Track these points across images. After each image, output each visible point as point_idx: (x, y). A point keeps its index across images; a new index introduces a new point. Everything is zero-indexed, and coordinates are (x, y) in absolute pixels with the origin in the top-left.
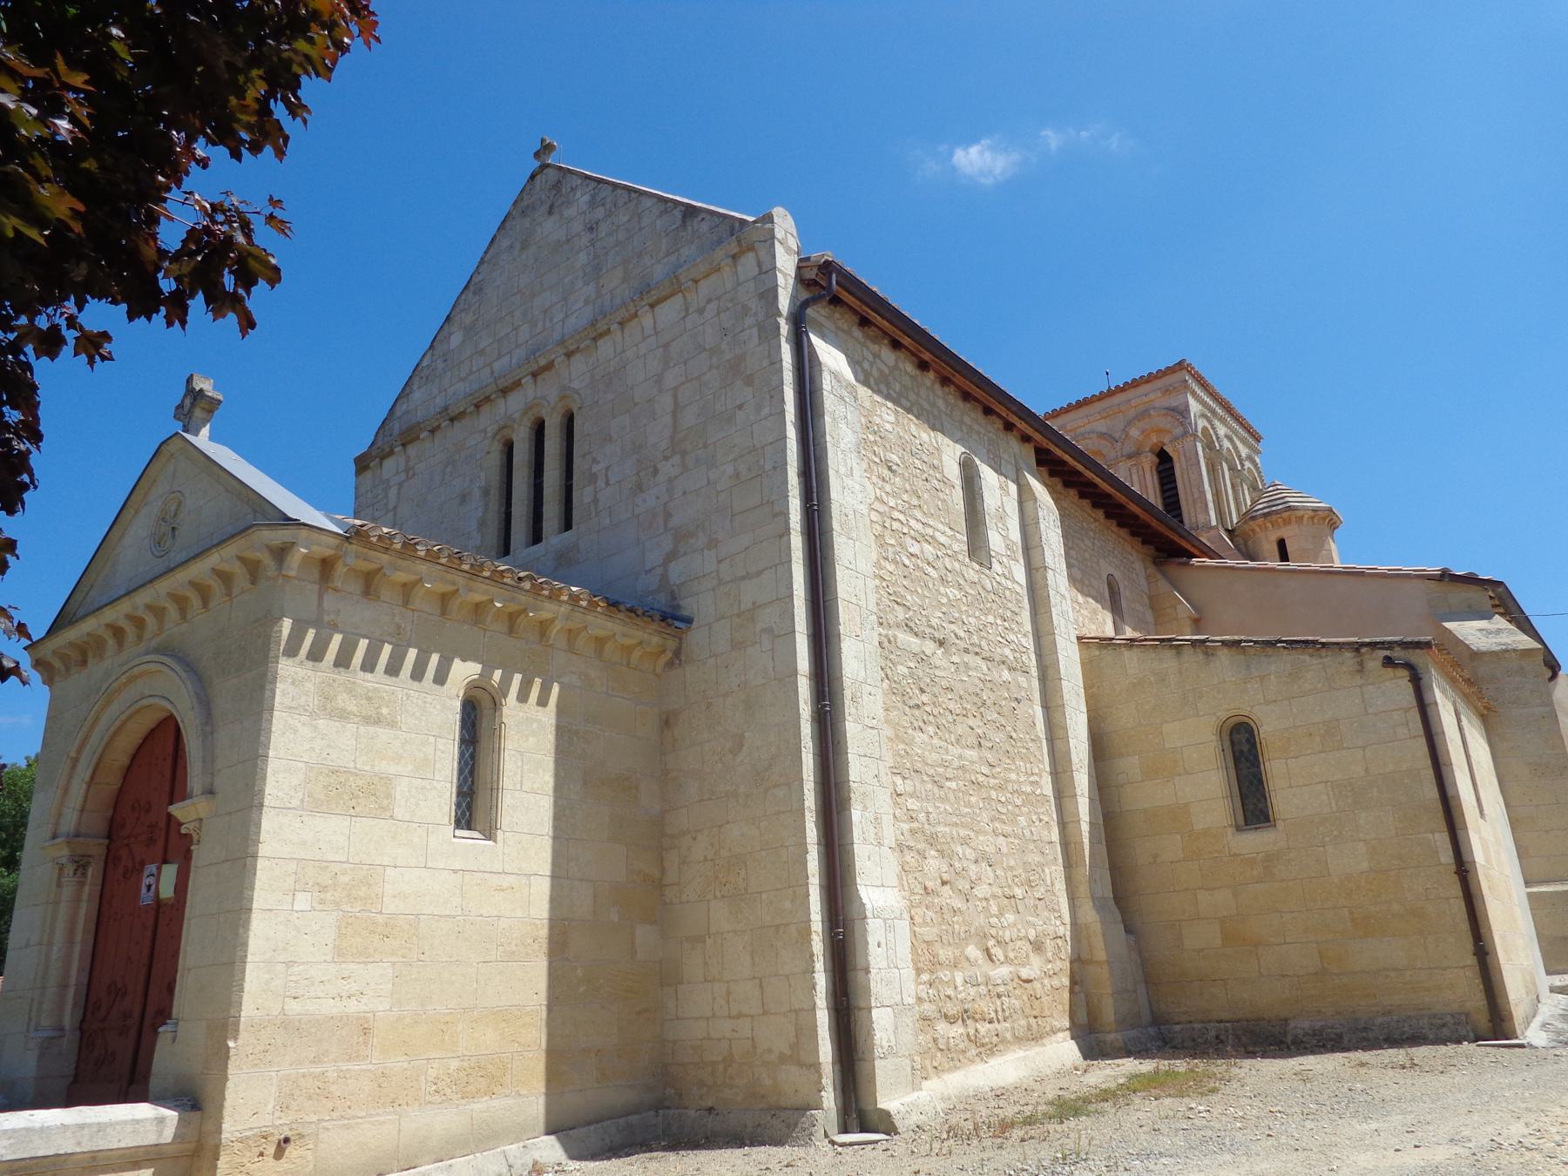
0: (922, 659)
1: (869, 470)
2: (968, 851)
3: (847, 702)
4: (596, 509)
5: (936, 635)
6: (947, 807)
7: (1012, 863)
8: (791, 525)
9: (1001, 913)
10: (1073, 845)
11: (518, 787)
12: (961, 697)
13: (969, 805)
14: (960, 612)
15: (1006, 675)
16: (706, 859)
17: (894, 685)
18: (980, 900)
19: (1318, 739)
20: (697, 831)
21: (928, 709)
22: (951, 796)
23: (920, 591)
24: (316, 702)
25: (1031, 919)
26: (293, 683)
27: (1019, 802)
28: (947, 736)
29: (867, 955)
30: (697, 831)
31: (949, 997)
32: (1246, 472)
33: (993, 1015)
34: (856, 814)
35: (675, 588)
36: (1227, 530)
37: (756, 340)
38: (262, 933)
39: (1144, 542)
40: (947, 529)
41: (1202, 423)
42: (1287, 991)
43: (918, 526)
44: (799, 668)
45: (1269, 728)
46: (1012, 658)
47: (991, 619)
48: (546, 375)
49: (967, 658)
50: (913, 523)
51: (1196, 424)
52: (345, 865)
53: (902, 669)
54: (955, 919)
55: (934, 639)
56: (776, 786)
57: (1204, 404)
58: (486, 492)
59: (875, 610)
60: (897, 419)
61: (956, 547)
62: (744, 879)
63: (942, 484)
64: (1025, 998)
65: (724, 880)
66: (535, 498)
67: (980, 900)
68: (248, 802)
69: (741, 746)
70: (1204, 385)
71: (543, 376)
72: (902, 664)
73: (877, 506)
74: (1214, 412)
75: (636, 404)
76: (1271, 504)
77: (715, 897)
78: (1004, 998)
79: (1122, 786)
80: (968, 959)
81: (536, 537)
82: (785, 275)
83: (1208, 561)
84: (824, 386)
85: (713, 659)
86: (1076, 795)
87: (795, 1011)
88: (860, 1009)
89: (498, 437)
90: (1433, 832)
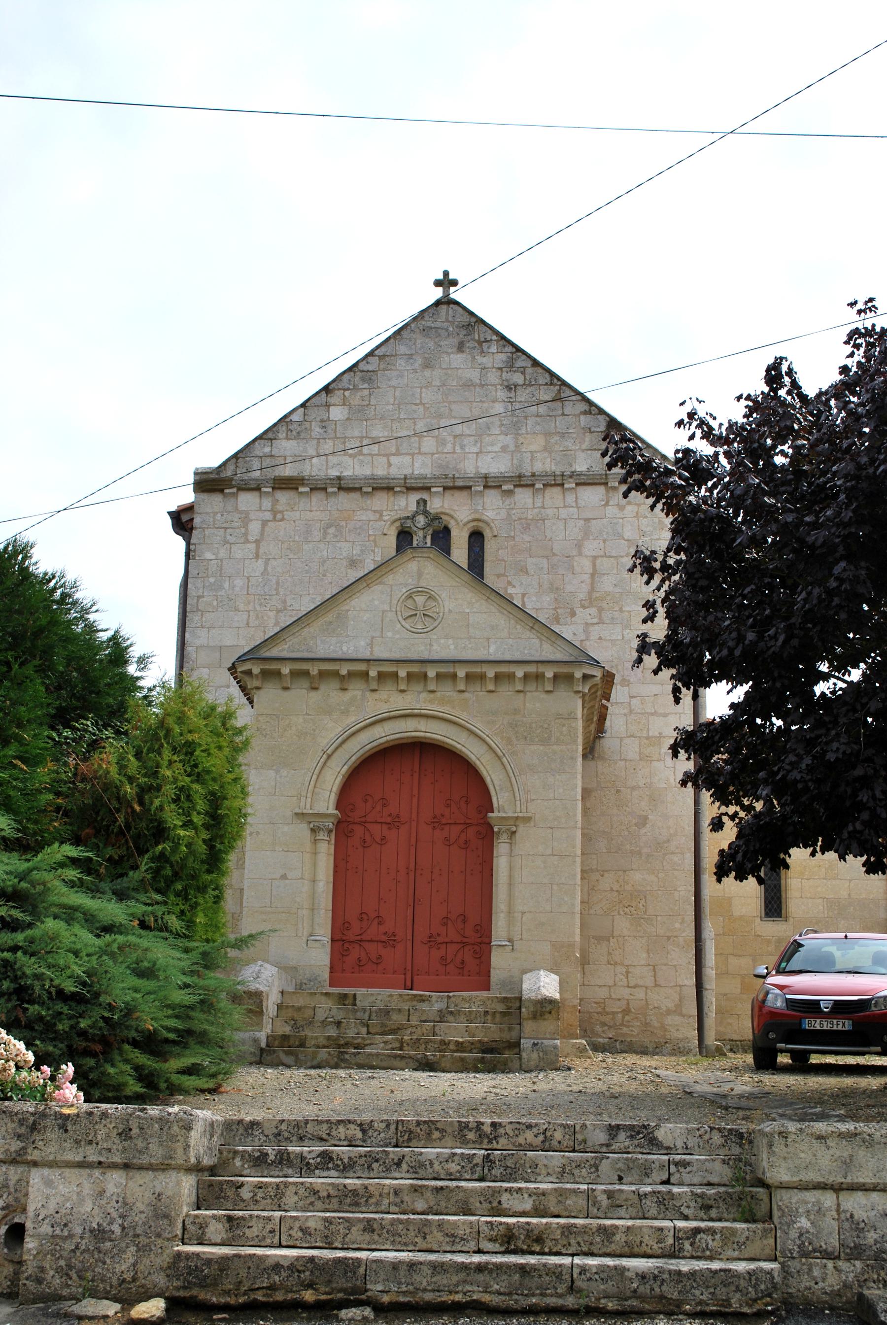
16: (612, 890)
30: (603, 871)
56: (672, 853)
69: (644, 825)
75: (554, 555)
77: (619, 914)
85: (623, 762)
87: (680, 986)
88: (706, 989)
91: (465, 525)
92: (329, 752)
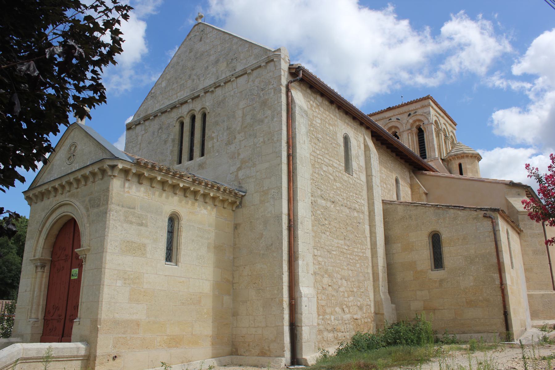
0: (326, 208)
1: (311, 141)
2: (338, 275)
3: (299, 224)
4: (213, 149)
5: (332, 200)
6: (332, 260)
7: (353, 280)
8: (283, 161)
9: (348, 297)
10: (375, 274)
11: (186, 248)
12: (339, 222)
13: (339, 260)
14: (341, 191)
15: (356, 214)
16: (248, 275)
17: (316, 218)
18: (342, 292)
19: (460, 240)
20: (245, 265)
21: (327, 226)
22: (334, 256)
23: (326, 184)
24: (123, 218)
25: (359, 299)
26: (116, 212)
27: (357, 259)
28: (333, 236)
29: (301, 309)
30: (245, 265)
31: (329, 323)
32: (450, 137)
33: (343, 330)
34: (300, 262)
35: (240, 180)
36: (441, 159)
37: (273, 93)
38: (107, 292)
39: (410, 165)
40: (338, 162)
41: (435, 118)
42: (443, 325)
43: (327, 161)
44: (283, 212)
45: (444, 236)
46: (358, 208)
47: (351, 194)
48: (197, 100)
49: (342, 208)
50: (325, 159)
51: (432, 119)
52: (131, 272)
53: (319, 212)
54: (333, 298)
55: (330, 201)
57: (436, 111)
58: (173, 140)
59: (310, 191)
60: (321, 121)
61: (341, 168)
62: (261, 282)
63: (336, 145)
64: (355, 325)
65: (254, 282)
66: (191, 143)
67: (342, 292)
68: (101, 250)
70: (437, 105)
71: (195, 100)
72: (319, 210)
73: (313, 153)
74: (440, 114)
76: (458, 150)
77: (251, 288)
78: (348, 325)
79: (394, 254)
80: (336, 312)
81: (191, 158)
82: (284, 71)
83: (432, 173)
84: (296, 112)
86: (377, 257)
87: (277, 326)
88: (298, 326)
89: (178, 121)
90: (495, 273)
91: (199, 112)
92: (458, 208)
